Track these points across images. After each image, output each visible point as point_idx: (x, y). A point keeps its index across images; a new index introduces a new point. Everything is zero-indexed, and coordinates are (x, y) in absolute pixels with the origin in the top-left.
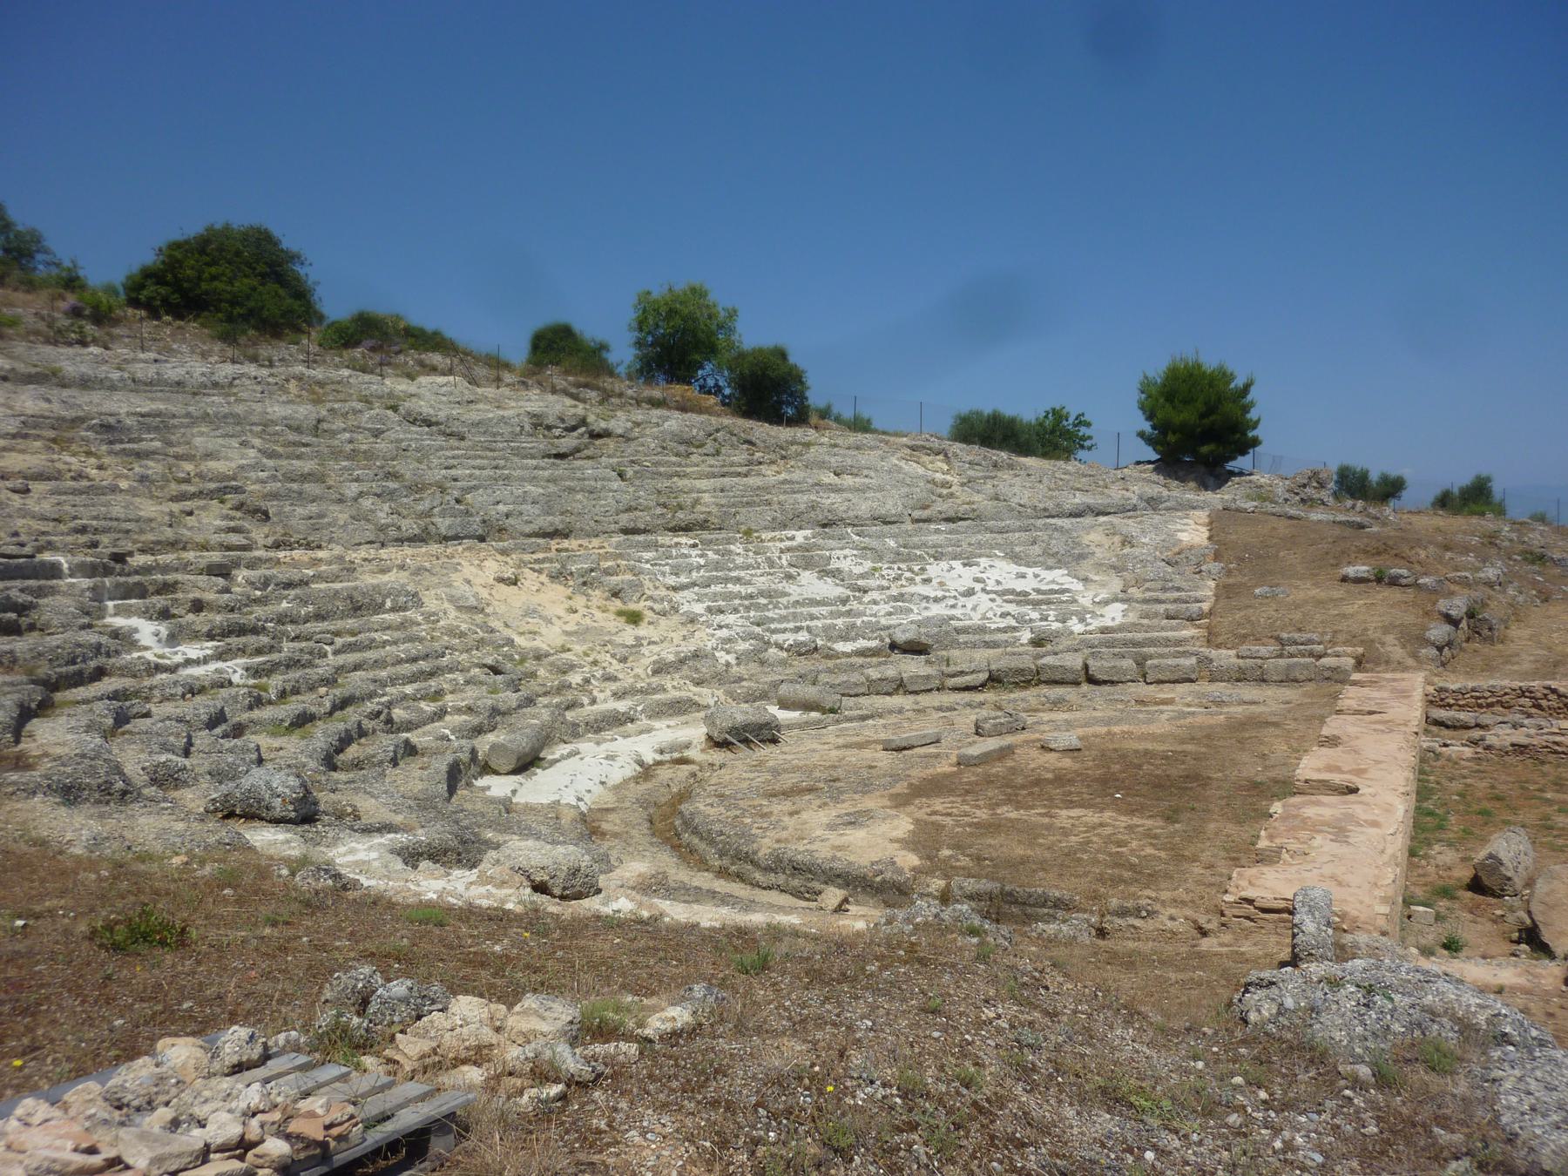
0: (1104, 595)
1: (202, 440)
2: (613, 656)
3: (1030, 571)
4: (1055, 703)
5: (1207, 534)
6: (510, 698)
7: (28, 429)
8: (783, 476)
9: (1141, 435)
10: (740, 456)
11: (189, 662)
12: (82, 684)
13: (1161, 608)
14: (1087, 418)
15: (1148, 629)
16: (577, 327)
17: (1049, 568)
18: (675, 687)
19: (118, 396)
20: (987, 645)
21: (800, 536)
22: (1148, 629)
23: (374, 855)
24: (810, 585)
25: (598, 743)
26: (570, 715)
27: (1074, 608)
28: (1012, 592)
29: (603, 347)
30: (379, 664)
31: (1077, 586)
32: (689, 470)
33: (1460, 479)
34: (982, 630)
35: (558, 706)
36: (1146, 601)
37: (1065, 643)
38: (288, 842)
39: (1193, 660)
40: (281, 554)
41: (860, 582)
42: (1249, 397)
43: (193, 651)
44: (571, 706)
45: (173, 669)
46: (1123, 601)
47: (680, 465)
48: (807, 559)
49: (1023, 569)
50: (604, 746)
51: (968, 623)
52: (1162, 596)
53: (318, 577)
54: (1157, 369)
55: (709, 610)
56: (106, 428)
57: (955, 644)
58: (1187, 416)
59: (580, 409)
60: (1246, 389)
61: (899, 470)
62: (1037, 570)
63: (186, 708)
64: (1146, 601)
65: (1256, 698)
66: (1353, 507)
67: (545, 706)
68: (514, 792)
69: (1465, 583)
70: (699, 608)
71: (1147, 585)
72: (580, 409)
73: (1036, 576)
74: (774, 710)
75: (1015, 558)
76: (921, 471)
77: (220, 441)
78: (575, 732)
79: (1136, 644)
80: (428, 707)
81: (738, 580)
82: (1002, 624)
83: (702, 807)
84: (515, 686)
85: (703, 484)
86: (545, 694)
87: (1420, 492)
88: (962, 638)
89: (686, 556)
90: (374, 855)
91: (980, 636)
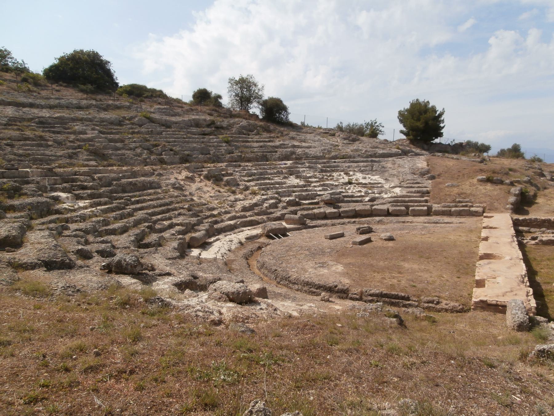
0: (393, 185)
1: (78, 127)
2: (228, 205)
3: (367, 176)
4: (378, 222)
5: (426, 164)
6: (194, 220)
7: (11, 122)
8: (281, 142)
9: (402, 132)
10: (265, 135)
11: (81, 208)
12: (115, 235)
13: (413, 190)
14: (383, 125)
15: (410, 197)
16: (209, 89)
17: (373, 175)
18: (250, 216)
19: (44, 110)
20: (354, 202)
21: (289, 163)
22: (410, 197)
23: (166, 286)
24: (293, 181)
25: (225, 236)
26: (215, 226)
27: (383, 189)
28: (361, 183)
29: (220, 97)
30: (174, 210)
31: (382, 181)
32: (249, 140)
33: (508, 146)
34: (352, 196)
35: (210, 222)
36: (407, 187)
37: (381, 201)
38: (136, 283)
39: (426, 208)
40: (110, 168)
41: (310, 180)
42: (442, 119)
43: (81, 204)
44: (216, 222)
45: (74, 210)
46: (400, 187)
47: (246, 138)
48: (291, 172)
49: (364, 176)
50: (228, 237)
51: (347, 194)
52: (413, 185)
53: (124, 177)
54: (438, 103)
55: (259, 189)
56: (41, 123)
57: (343, 201)
58: (420, 124)
59: (212, 118)
60: (441, 115)
61: (320, 141)
62: (369, 176)
63: (82, 225)
64: (407, 187)
65: (449, 221)
66: (475, 155)
67: (206, 223)
68: (200, 254)
69: (518, 182)
70: (256, 188)
71: (408, 182)
72: (212, 118)
73: (369, 178)
74: (284, 223)
75: (362, 172)
76: (328, 141)
77: (84, 127)
78: (220, 231)
79: (405, 202)
80: (166, 223)
81: (269, 179)
82: (359, 194)
83: (267, 260)
84: (195, 215)
85: (256, 145)
86: (206, 218)
87: (493, 152)
88: (346, 199)
89: (250, 170)
90: (166, 286)
91: (352, 199)
